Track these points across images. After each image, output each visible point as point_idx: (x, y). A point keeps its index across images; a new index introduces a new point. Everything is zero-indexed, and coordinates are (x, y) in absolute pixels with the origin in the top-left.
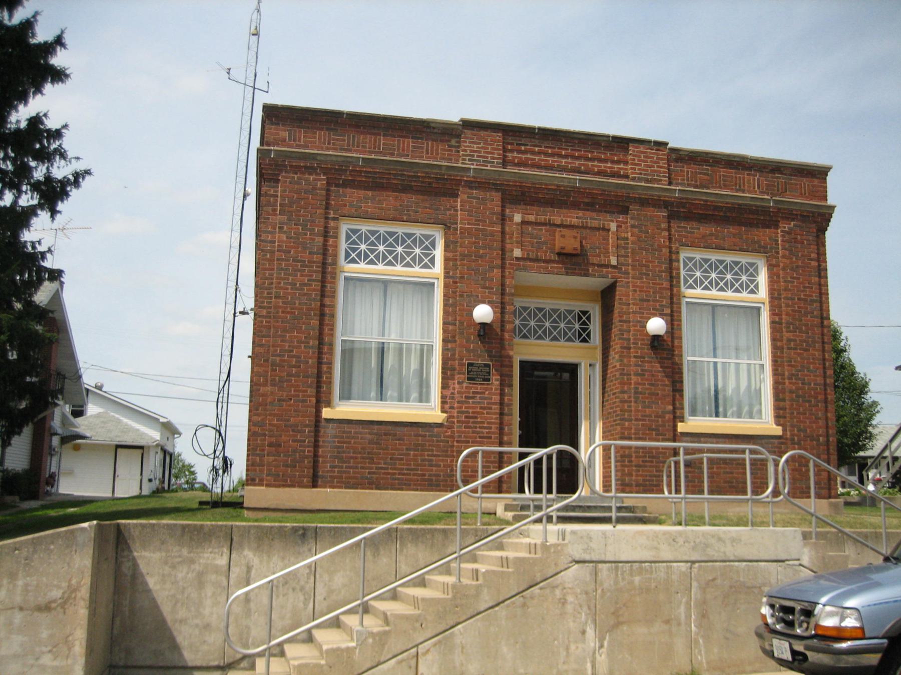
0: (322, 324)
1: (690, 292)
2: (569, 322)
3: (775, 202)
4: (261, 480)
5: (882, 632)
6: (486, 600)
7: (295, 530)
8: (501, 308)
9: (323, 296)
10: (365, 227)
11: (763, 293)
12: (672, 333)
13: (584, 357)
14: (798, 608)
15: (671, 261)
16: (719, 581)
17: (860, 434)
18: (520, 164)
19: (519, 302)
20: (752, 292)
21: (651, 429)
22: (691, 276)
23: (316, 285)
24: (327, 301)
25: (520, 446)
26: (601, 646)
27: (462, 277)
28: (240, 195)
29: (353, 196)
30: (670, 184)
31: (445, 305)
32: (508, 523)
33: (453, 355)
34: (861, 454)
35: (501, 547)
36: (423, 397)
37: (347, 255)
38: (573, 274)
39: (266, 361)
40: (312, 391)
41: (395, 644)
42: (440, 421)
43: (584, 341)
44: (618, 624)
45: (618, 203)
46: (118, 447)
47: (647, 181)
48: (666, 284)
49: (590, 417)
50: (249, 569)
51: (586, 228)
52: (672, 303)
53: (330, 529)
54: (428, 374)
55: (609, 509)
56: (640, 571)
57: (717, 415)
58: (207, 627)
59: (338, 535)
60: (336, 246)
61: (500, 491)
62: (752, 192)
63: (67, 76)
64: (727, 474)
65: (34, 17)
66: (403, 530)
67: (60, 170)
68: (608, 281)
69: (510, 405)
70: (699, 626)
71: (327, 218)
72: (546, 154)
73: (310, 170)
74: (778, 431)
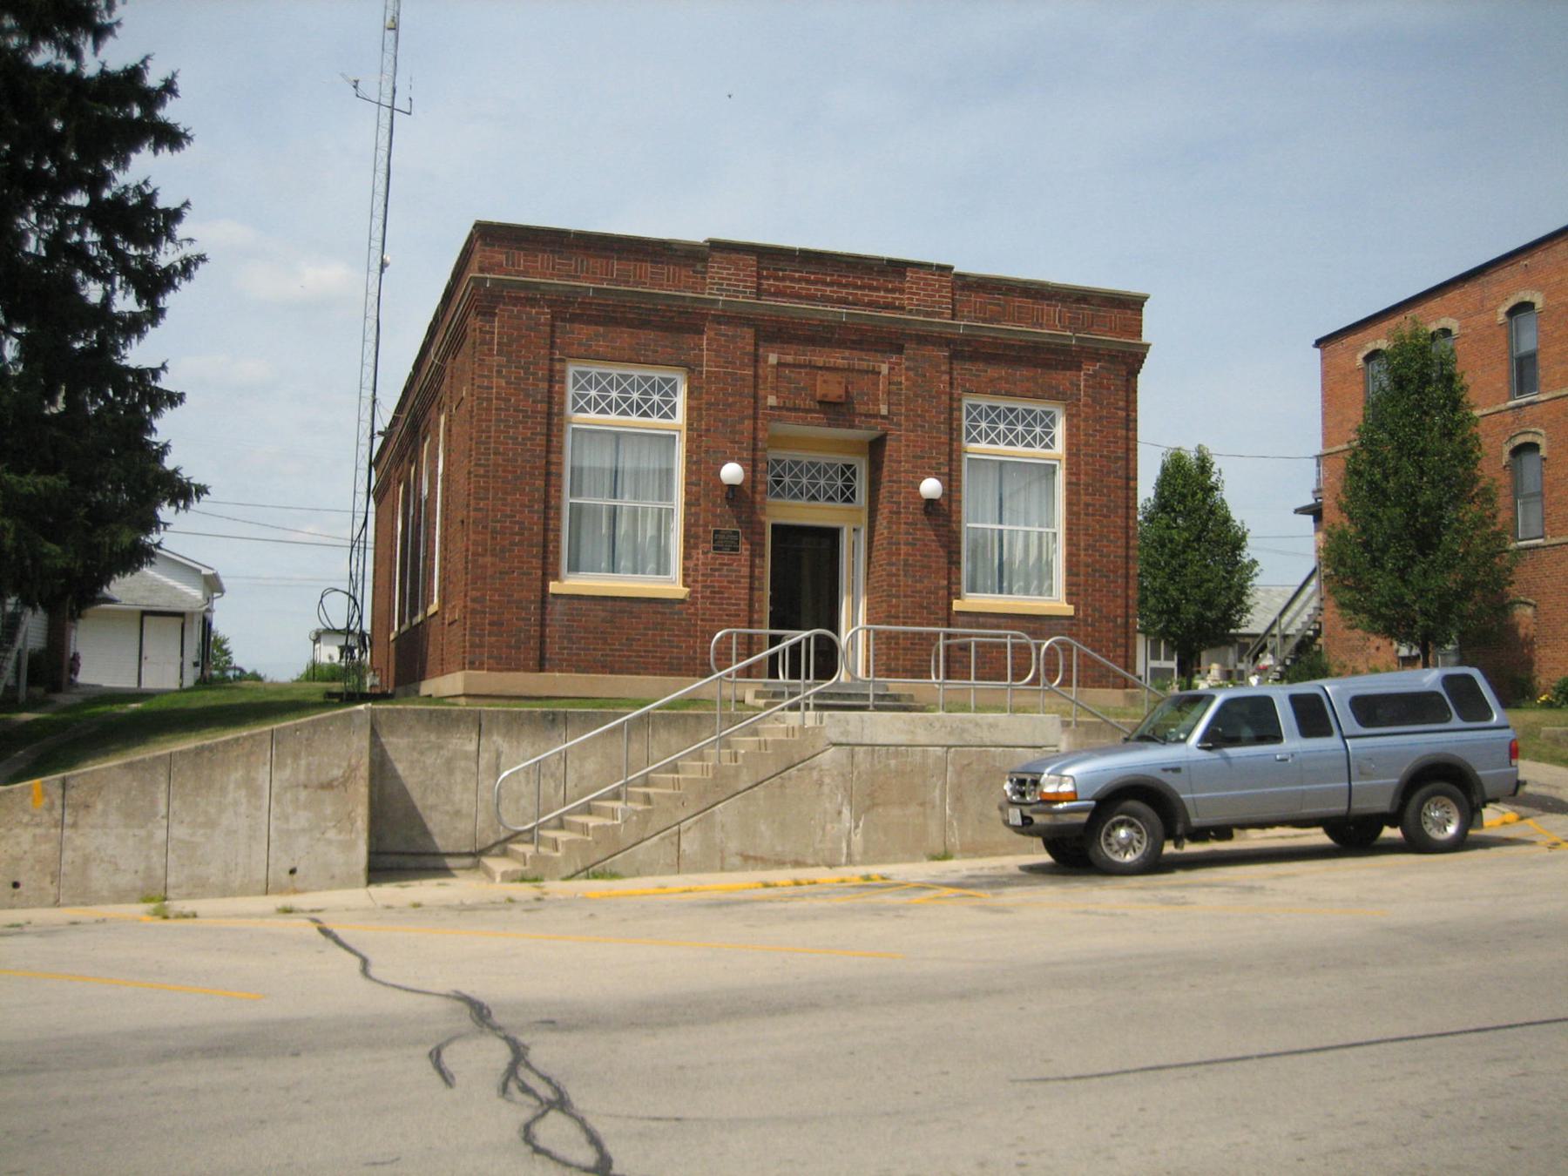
0: (547, 485)
1: (973, 446)
2: (831, 478)
3: (1078, 339)
4: (482, 664)
5: (1091, 794)
6: (745, 780)
7: (545, 715)
8: (752, 466)
9: (548, 452)
10: (595, 369)
11: (1060, 448)
12: (950, 496)
13: (847, 519)
14: (1029, 779)
15: (951, 409)
16: (975, 766)
17: (1231, 606)
18: (778, 293)
19: (773, 455)
20: (1047, 446)
21: (922, 607)
22: (975, 428)
23: (541, 440)
24: (553, 458)
25: (771, 627)
26: (857, 827)
27: (708, 430)
28: (377, 267)
29: (583, 332)
30: (953, 317)
31: (688, 463)
32: (761, 710)
33: (697, 521)
34: (1232, 631)
35: (755, 733)
36: (662, 568)
37: (575, 402)
38: (838, 426)
39: (485, 527)
40: (537, 562)
41: (658, 822)
42: (681, 596)
43: (848, 500)
44: (874, 805)
45: (891, 341)
46: (144, 613)
47: (927, 314)
48: (944, 438)
49: (853, 591)
50: (499, 756)
51: (853, 370)
52: (951, 460)
53: (580, 714)
54: (667, 538)
55: (866, 696)
56: (896, 755)
57: (1001, 592)
58: (457, 813)
59: (589, 721)
60: (563, 393)
61: (749, 676)
62: (1051, 328)
63: (189, 139)
64: (992, 657)
65: (143, 62)
66: (654, 716)
67: (167, 256)
68: (874, 434)
69: (761, 578)
70: (953, 809)
71: (552, 360)
72: (808, 281)
73: (532, 302)
74: (1069, 610)
